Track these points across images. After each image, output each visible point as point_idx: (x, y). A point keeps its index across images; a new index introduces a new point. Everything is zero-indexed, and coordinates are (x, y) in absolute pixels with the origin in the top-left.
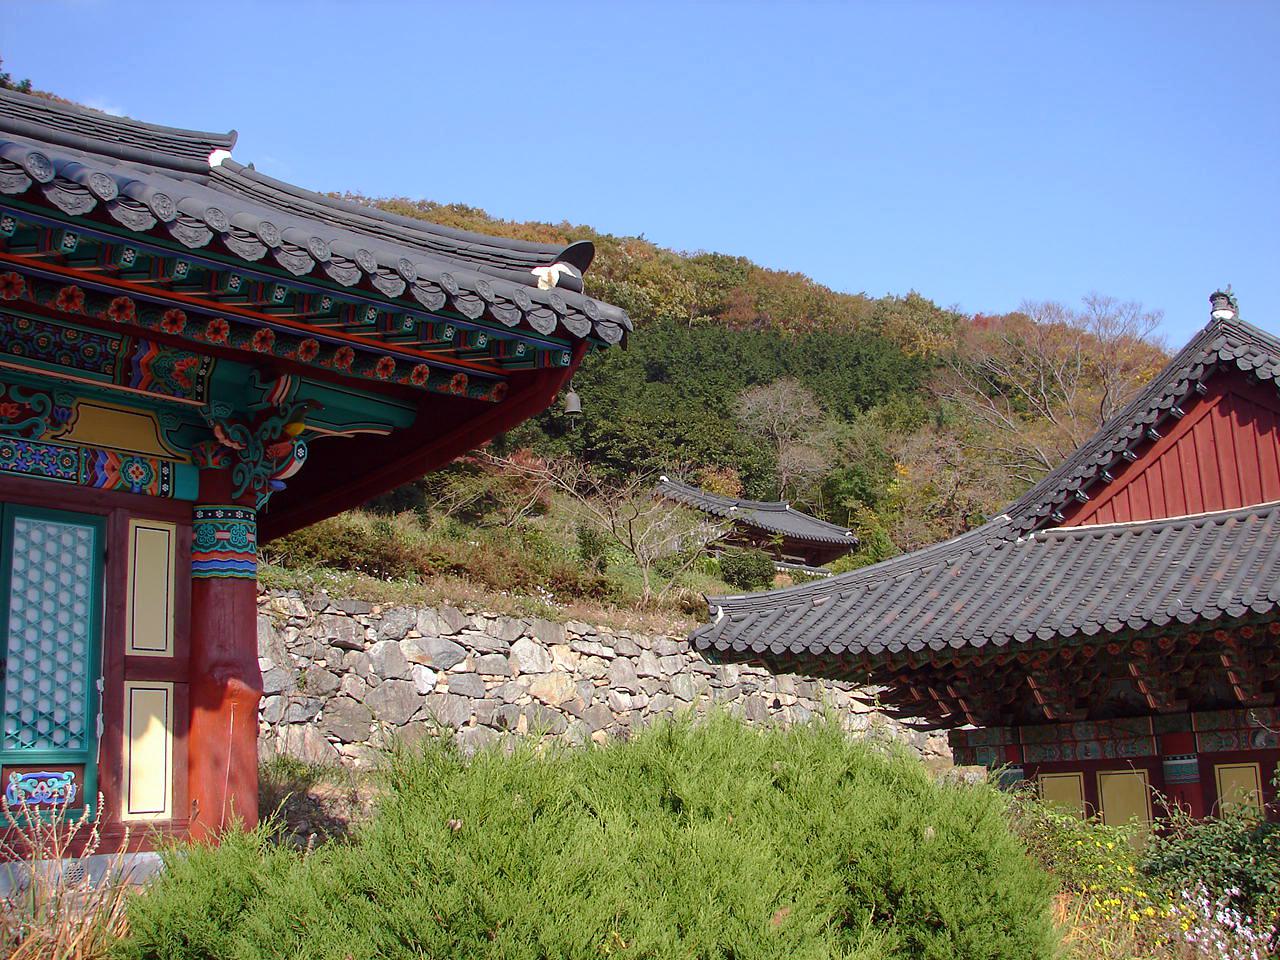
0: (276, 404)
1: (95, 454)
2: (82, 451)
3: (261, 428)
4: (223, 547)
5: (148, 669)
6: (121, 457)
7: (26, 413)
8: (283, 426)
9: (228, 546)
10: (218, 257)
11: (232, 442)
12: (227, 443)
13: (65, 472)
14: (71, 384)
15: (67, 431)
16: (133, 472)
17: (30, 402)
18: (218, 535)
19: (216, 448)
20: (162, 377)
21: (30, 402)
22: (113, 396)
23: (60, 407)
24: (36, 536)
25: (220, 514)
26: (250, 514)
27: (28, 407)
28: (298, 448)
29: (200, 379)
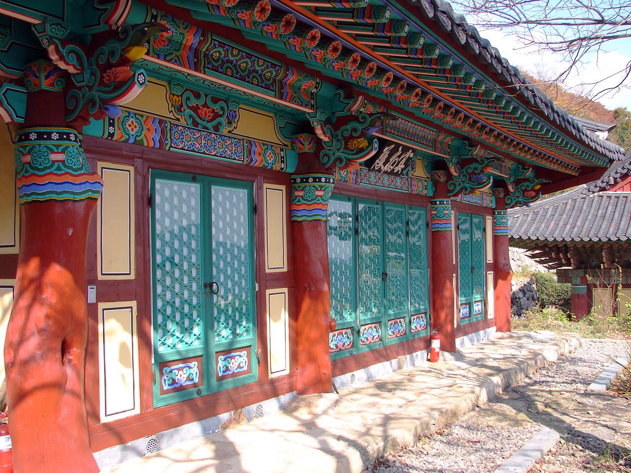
0: (114, 27)
2: (245, 141)
3: (97, 52)
4: (299, 201)
8: (123, 50)
9: (62, 167)
11: (67, 64)
12: (62, 66)
13: (235, 156)
16: (130, 125)
17: (217, 107)
18: (53, 157)
19: (49, 69)
21: (217, 107)
22: (265, 105)
23: (231, 111)
24: (167, 193)
25: (55, 136)
26: (443, 201)
27: (216, 111)
28: (139, 74)
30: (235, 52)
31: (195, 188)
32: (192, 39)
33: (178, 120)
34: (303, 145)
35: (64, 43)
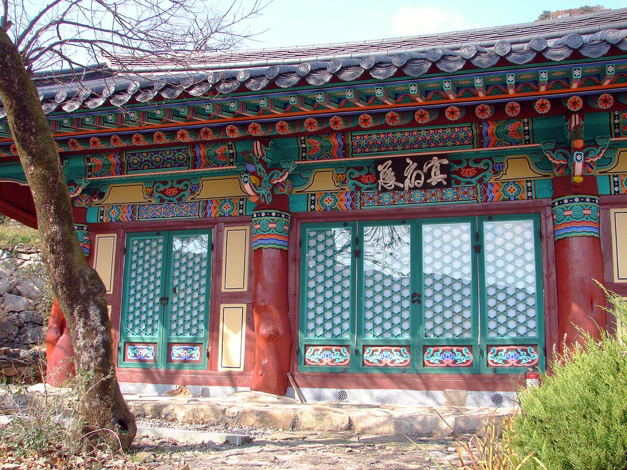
1: (207, 202)
4: (587, 219)
5: (234, 297)
6: (500, 184)
7: (180, 191)
10: (617, 57)
14: (143, 177)
15: (503, 174)
20: (502, 137)
22: (322, 165)
23: (497, 164)
25: (588, 200)
29: (526, 133)
30: (145, 155)
31: (466, 227)
32: (114, 160)
33: (150, 201)
34: (284, 188)
35: (553, 151)
